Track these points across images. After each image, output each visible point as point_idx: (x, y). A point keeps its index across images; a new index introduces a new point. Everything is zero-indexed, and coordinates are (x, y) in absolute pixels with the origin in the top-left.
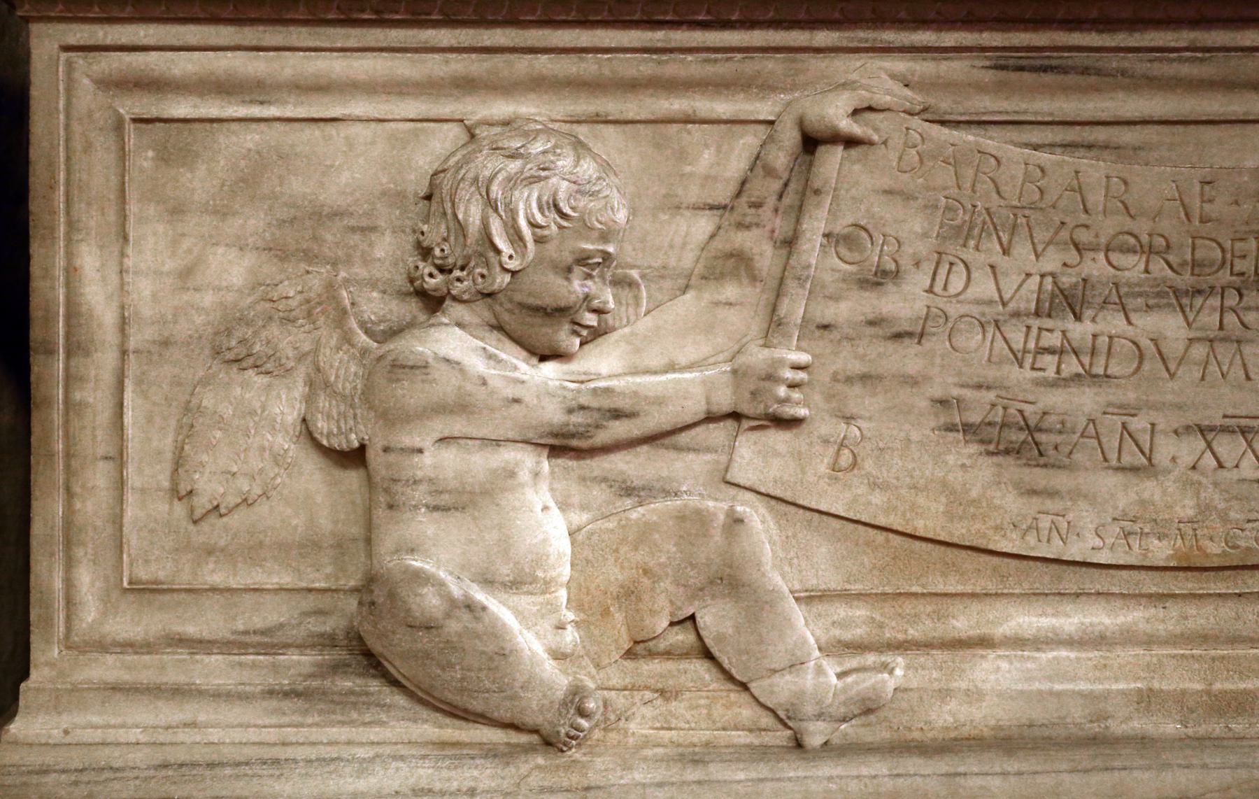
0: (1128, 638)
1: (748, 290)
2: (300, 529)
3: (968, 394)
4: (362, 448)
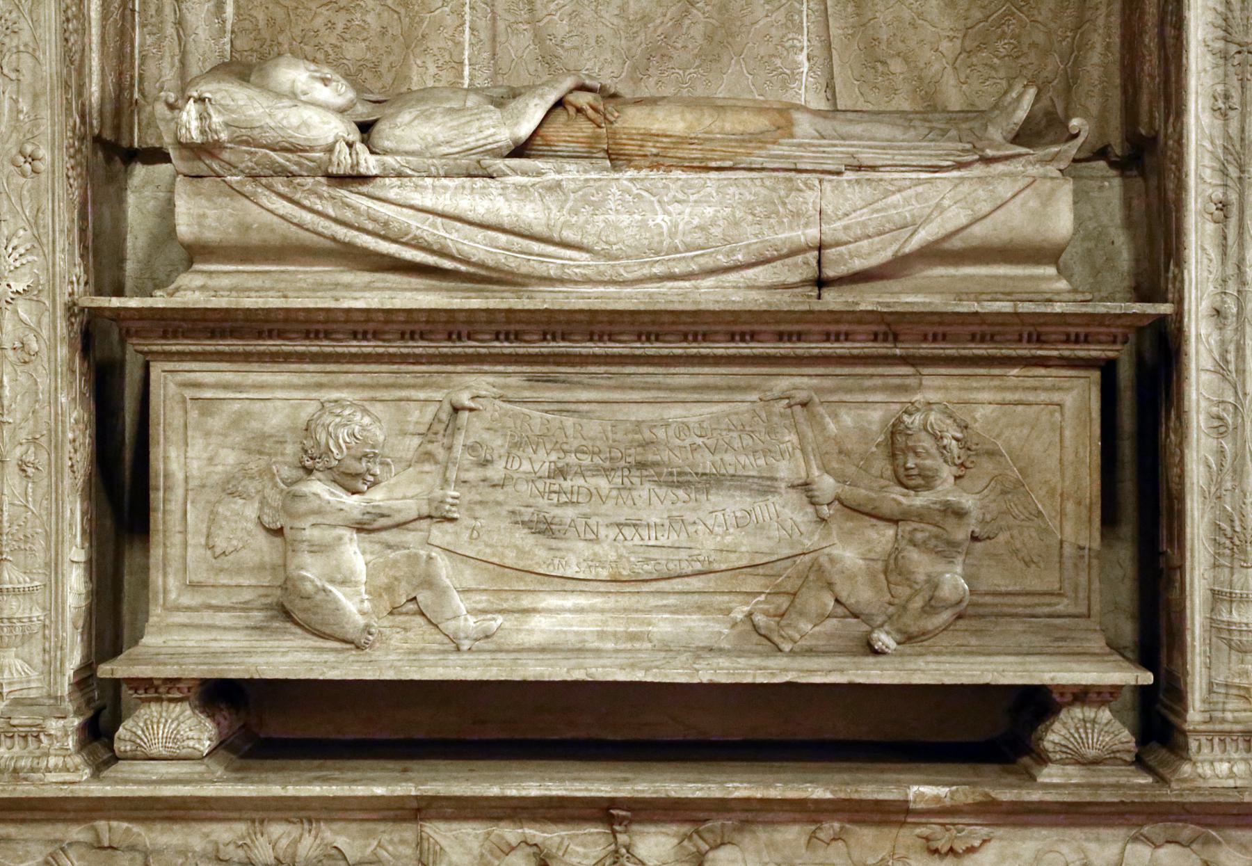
0: (593, 610)
1: (434, 467)
3: (523, 509)
4: (281, 529)
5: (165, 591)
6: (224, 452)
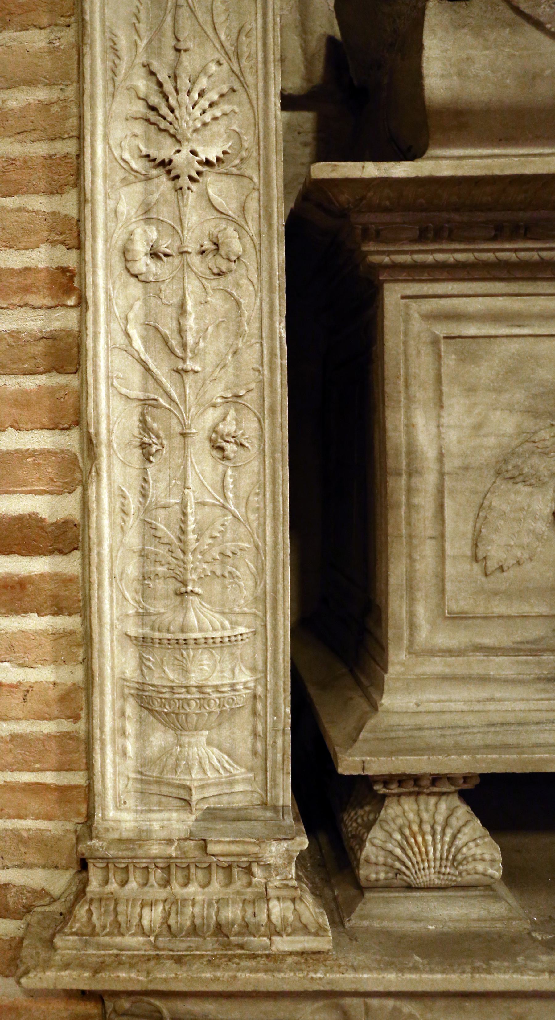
2: (551, 579)
5: (412, 626)
6: (497, 416)
